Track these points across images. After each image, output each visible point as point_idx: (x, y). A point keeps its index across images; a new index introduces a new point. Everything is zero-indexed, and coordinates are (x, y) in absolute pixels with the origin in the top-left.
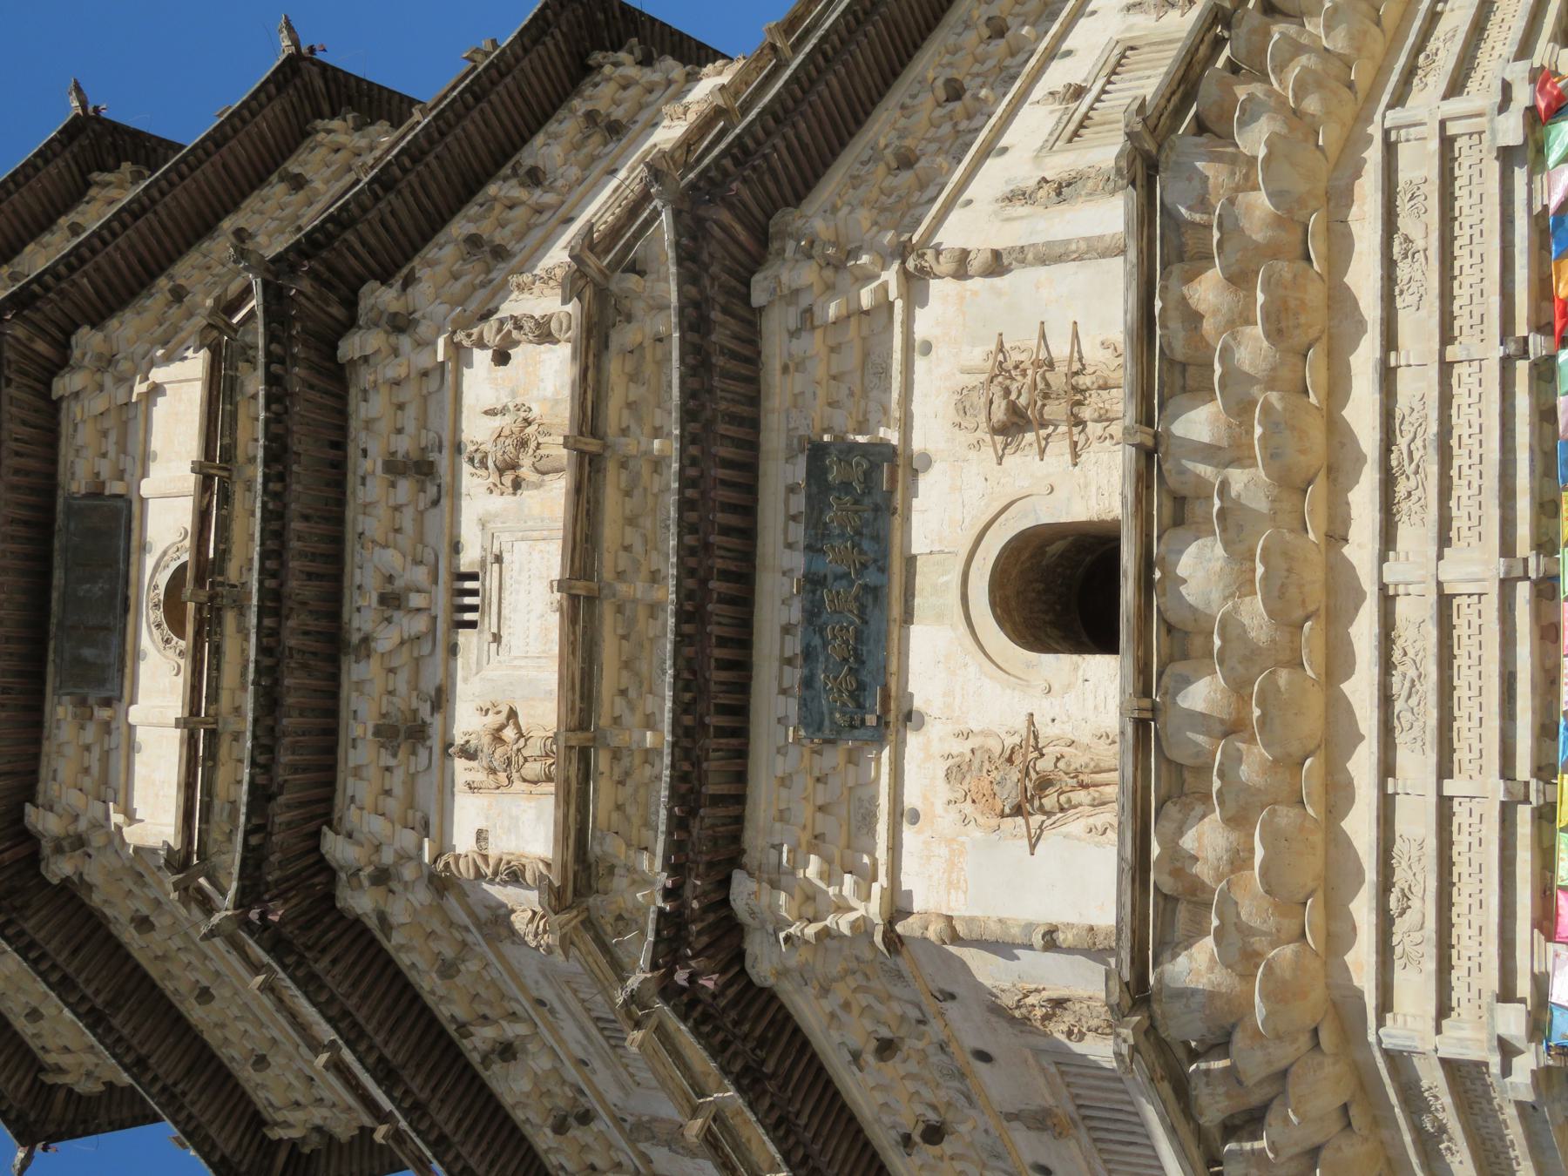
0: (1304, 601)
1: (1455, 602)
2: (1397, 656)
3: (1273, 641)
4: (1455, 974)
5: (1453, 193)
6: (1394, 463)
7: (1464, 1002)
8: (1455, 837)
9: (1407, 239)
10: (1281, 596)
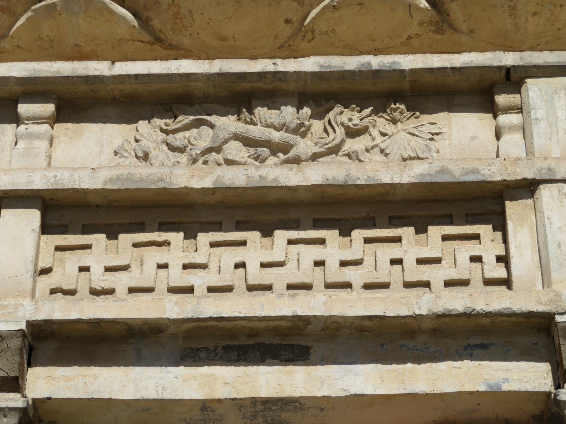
1: (485, 230)
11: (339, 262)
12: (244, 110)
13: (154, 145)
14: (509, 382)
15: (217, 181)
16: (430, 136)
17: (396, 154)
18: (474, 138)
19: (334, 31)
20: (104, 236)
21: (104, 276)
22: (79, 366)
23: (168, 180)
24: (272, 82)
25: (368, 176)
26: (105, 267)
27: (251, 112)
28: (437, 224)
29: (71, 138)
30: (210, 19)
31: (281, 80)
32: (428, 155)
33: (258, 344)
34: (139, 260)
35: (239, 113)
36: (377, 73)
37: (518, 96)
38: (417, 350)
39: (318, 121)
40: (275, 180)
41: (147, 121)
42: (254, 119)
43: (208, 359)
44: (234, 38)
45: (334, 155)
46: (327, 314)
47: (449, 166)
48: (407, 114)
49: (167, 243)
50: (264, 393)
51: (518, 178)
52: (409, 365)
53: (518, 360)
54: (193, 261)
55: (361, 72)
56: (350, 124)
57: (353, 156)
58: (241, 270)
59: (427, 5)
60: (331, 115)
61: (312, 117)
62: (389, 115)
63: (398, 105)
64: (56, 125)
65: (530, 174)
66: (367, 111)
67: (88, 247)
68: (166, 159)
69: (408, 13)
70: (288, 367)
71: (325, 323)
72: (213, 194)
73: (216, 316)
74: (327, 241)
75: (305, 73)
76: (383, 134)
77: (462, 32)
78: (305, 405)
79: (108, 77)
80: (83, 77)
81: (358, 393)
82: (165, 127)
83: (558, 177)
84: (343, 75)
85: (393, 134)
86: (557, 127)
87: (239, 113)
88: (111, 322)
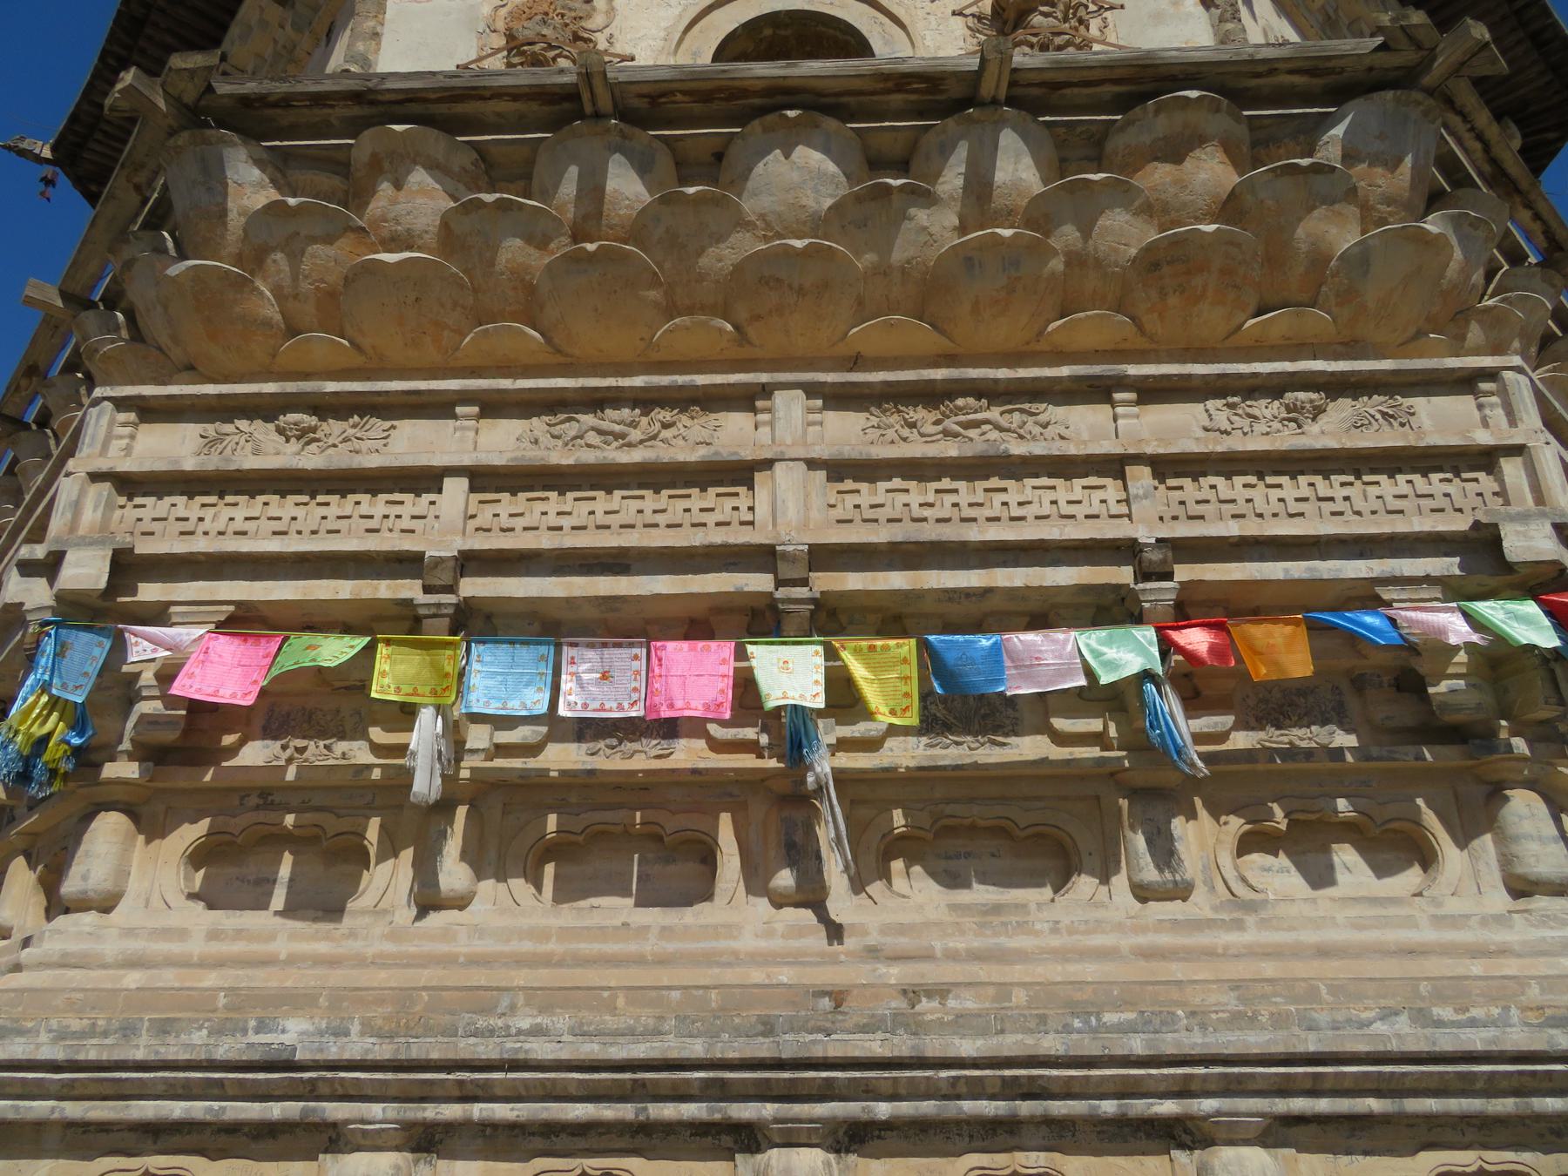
0: (758, 317)
1: (742, 490)
3: (701, 278)
4: (181, 500)
5: (1400, 471)
6: (960, 402)
7: (139, 513)
8: (383, 497)
9: (1318, 412)
15: (576, 460)
18: (741, 429)
35: (595, 412)
36: (681, 387)
49: (547, 499)
61: (641, 415)
65: (769, 456)
66: (676, 411)
87: (595, 412)
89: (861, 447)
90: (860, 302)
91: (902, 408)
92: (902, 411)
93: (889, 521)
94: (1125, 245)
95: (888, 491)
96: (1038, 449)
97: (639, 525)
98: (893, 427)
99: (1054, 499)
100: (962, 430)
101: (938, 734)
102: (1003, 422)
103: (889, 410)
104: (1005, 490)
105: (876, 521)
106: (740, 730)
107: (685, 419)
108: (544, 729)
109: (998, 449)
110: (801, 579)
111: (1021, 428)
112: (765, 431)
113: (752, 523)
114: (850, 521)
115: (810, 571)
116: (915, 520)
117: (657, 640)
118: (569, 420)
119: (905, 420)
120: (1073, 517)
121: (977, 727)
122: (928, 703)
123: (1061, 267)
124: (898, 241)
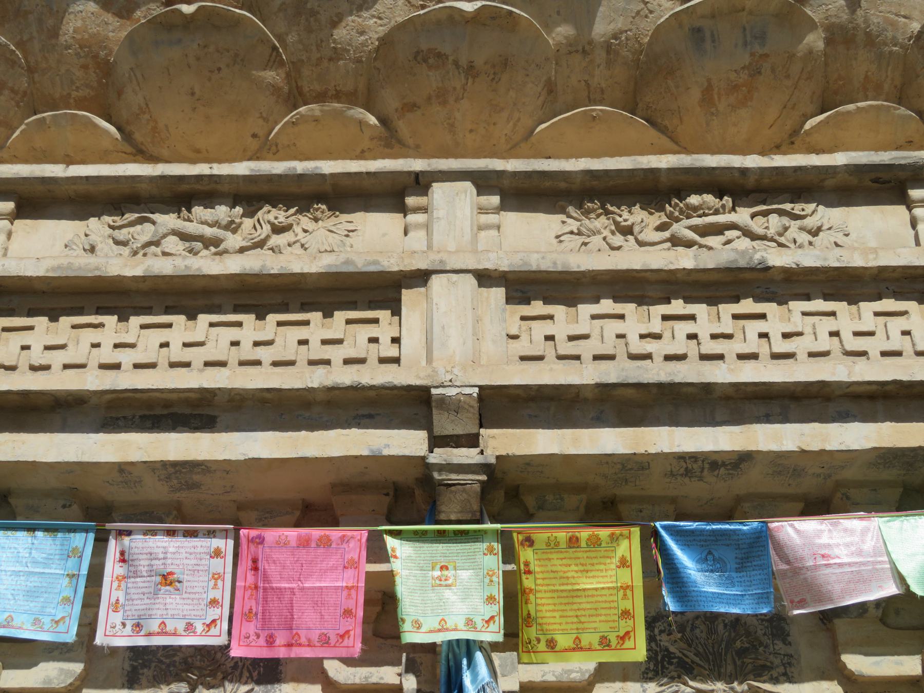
1: (384, 315)
2: (272, 214)
3: (337, 54)
6: (694, 200)
10: (421, 57)
11: (252, 343)
12: (183, 209)
13: (101, 239)
14: (389, 448)
15: (146, 270)
16: (346, 233)
17: (314, 248)
18: (384, 235)
19: (294, 144)
20: (46, 319)
21: (43, 354)
22: (10, 432)
23: (104, 269)
24: (209, 184)
25: (282, 267)
26: (44, 346)
27: (189, 211)
28: (342, 310)
29: (28, 233)
30: (184, 133)
31: (216, 182)
32: (342, 249)
33: (172, 414)
34: (76, 340)
35: (179, 212)
36: (301, 177)
37: (425, 198)
38: (312, 419)
39: (249, 219)
40: (199, 269)
41: (97, 218)
42: (191, 216)
43: (125, 427)
44: (207, 150)
45: (259, 249)
46: (230, 387)
47: (354, 258)
48: (328, 213)
49: (101, 325)
50: (172, 457)
51: (413, 269)
52: (303, 433)
53: (399, 428)
54: (123, 341)
55: (286, 175)
56: (276, 222)
57: (276, 250)
58: (165, 349)
59: (377, 122)
60: (260, 214)
61: (243, 216)
62: (312, 214)
63: (320, 205)
64: (16, 222)
65: (423, 265)
66: (292, 211)
67: (31, 328)
68: (110, 251)
69: (359, 128)
70: (196, 434)
71: (230, 395)
72: (144, 282)
73: (131, 388)
74: (244, 324)
75: (237, 176)
76: (305, 231)
77: (409, 147)
78: (211, 467)
79: (62, 179)
80: (39, 178)
81: (255, 457)
82: (112, 224)
83: (448, 268)
84: (270, 178)
85: (314, 230)
86: (455, 225)
87: (179, 212)
88: (38, 393)
89: (554, 256)
90: (551, 89)
91: (611, 208)
92: (613, 213)
93: (596, 358)
94: (905, 17)
95: (594, 317)
96: (809, 259)
97: (233, 361)
98: (599, 232)
99: (834, 329)
100: (696, 237)
101: (672, 679)
102: (757, 226)
103: (594, 210)
104: (763, 316)
105: (577, 358)
106: (373, 670)
107: (305, 221)
108: (78, 668)
109: (751, 258)
110: (468, 436)
111: (781, 235)
112: (417, 239)
113: (396, 360)
114: (540, 358)
115: (481, 426)
116: (633, 357)
117: (250, 526)
118: (141, 221)
119: (616, 224)
120: (863, 354)
121: (730, 668)
122: (656, 631)
123: (821, 45)
124: (601, 9)
